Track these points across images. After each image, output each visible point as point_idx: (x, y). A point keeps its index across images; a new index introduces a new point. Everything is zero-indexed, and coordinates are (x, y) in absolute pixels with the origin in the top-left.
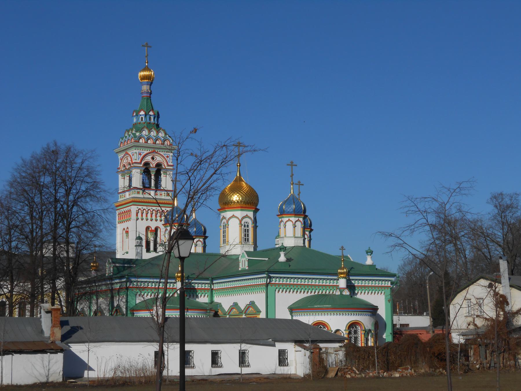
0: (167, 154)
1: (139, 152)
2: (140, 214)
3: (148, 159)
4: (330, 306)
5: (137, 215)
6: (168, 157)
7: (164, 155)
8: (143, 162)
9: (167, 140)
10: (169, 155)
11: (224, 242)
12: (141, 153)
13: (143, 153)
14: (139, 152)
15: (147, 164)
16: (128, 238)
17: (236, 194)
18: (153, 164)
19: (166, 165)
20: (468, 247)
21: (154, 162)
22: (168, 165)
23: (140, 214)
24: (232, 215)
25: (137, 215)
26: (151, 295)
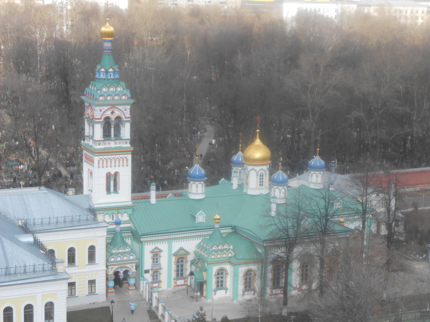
0: (124, 108)
1: (99, 109)
2: (101, 163)
3: (108, 113)
4: (104, 39)
5: (99, 164)
6: (125, 110)
7: (122, 109)
8: (103, 117)
9: (104, 96)
10: (127, 108)
11: (262, 176)
12: (102, 110)
13: (104, 109)
14: (99, 109)
15: (107, 119)
16: (73, 195)
17: (257, 158)
18: (113, 118)
19: (124, 118)
20: (366, 122)
21: (113, 116)
22: (126, 118)
23: (101, 163)
24: (261, 168)
25: (99, 164)
26: (156, 255)
